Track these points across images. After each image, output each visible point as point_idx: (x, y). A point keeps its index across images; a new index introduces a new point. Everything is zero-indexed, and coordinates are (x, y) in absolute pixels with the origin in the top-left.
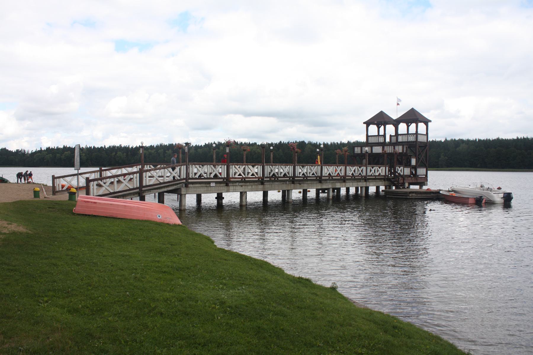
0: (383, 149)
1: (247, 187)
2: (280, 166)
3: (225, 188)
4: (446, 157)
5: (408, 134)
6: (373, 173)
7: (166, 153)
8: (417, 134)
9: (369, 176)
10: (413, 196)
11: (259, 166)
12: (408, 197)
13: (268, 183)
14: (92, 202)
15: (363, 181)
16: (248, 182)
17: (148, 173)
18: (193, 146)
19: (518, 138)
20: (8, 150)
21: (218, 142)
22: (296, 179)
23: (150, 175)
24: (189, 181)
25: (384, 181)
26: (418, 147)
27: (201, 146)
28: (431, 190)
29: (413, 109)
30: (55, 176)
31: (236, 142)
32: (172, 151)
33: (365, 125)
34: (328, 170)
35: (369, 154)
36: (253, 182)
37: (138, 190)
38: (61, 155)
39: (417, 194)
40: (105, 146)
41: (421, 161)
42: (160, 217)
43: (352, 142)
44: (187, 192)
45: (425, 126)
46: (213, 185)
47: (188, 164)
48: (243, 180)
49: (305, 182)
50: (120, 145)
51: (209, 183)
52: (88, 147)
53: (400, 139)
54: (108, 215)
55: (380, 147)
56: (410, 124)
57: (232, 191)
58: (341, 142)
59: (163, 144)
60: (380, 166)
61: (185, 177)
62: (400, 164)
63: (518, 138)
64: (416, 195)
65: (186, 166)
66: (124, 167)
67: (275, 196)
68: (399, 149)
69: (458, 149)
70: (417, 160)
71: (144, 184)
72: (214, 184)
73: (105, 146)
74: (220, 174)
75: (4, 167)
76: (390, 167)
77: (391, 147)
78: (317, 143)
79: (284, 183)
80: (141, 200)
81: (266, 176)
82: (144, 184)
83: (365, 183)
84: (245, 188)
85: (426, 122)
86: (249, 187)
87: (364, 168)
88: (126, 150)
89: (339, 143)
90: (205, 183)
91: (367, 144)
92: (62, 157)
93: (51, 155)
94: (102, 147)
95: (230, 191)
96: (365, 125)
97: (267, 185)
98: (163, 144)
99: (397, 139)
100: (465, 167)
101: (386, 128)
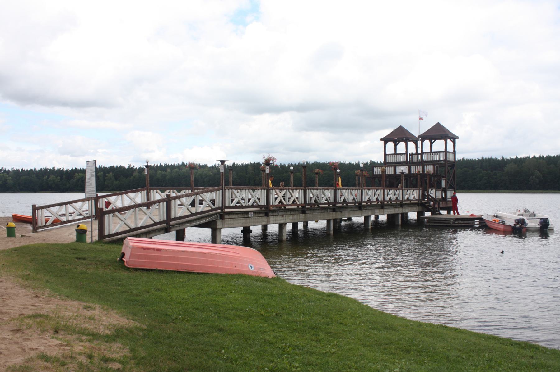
0: (410, 170)
1: (288, 218)
2: (310, 190)
3: (265, 219)
5: (396, 154)
7: (106, 176)
8: (446, 152)
9: (405, 201)
10: (460, 223)
11: (301, 190)
13: (309, 212)
14: (154, 249)
15: (399, 206)
16: (289, 211)
17: (177, 200)
18: (136, 168)
19: (482, 158)
21: (165, 164)
22: (337, 205)
23: (179, 203)
24: (226, 210)
25: (418, 206)
26: (447, 166)
28: (475, 216)
30: (37, 206)
31: (184, 164)
32: (113, 175)
35: (406, 175)
36: (294, 211)
37: (165, 224)
39: (463, 221)
40: (35, 168)
41: (450, 184)
42: (253, 268)
43: (311, 163)
44: (223, 225)
45: (414, 145)
46: (251, 215)
47: (224, 188)
49: (345, 210)
50: (53, 168)
51: (247, 213)
52: (16, 170)
54: (180, 269)
55: (405, 167)
56: (433, 141)
57: (273, 222)
58: (503, 158)
59: (103, 167)
62: (432, 186)
63: (482, 158)
64: (462, 222)
66: (126, 193)
68: (430, 169)
71: (173, 217)
72: (253, 213)
73: (35, 168)
74: (259, 199)
75: (552, 193)
78: (154, 165)
79: (325, 211)
80: (177, 239)
81: (308, 203)
82: (173, 217)
83: (401, 209)
84: (286, 218)
85: (454, 139)
86: (290, 218)
87: (401, 191)
88: (60, 173)
89: (297, 164)
90: (243, 213)
91: (386, 164)
94: (31, 170)
95: (271, 222)
96: (383, 142)
97: (309, 215)
98: (103, 167)
101: (408, 145)
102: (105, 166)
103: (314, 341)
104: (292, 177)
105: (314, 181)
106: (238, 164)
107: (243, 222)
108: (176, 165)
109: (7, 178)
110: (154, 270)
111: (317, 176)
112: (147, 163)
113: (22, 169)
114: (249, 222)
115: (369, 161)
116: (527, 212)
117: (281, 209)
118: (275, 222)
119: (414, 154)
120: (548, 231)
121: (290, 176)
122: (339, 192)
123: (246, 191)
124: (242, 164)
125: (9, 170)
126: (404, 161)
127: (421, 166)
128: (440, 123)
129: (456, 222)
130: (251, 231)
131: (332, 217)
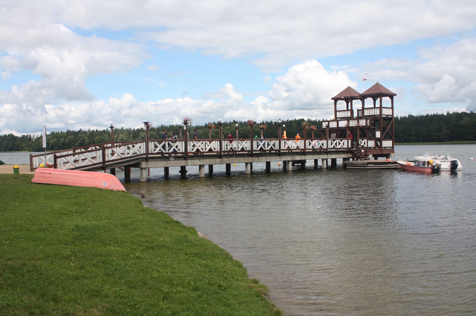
1: (205, 161)
3: (184, 162)
4: (448, 131)
6: (342, 146)
12: (366, 168)
14: (47, 173)
20: (14, 136)
24: (149, 156)
27: (202, 126)
29: (377, 84)
33: (334, 100)
34: (292, 144)
37: (102, 165)
38: (65, 139)
41: (387, 133)
42: (106, 185)
48: (202, 154)
53: (366, 113)
59: (164, 126)
60: (342, 139)
61: (145, 153)
62: (363, 136)
65: (146, 142)
67: (220, 168)
68: (363, 123)
69: (460, 122)
70: (382, 132)
72: (173, 158)
76: (352, 141)
77: (355, 121)
78: (316, 120)
84: (203, 161)
85: (391, 96)
86: (207, 161)
92: (66, 141)
93: (55, 139)
96: (333, 101)
98: (164, 126)
99: (363, 113)
100: (468, 140)
102: (166, 126)
103: (219, 254)
104: (237, 132)
105: (235, 134)
106: (284, 121)
107: (163, 164)
108: (228, 123)
109: (85, 138)
110: (46, 184)
111: (262, 130)
112: (112, 125)
113: (97, 130)
114: (170, 164)
115: (233, 120)
116: (440, 156)
117: (198, 155)
118: (193, 164)
119: (360, 110)
120: (457, 171)
121: (236, 131)
122: (282, 142)
123: (180, 142)
124: (287, 121)
125: (86, 131)
126: (348, 116)
127: (357, 120)
128: (379, 83)
129: (368, 166)
130: (187, 172)
131: (249, 161)
